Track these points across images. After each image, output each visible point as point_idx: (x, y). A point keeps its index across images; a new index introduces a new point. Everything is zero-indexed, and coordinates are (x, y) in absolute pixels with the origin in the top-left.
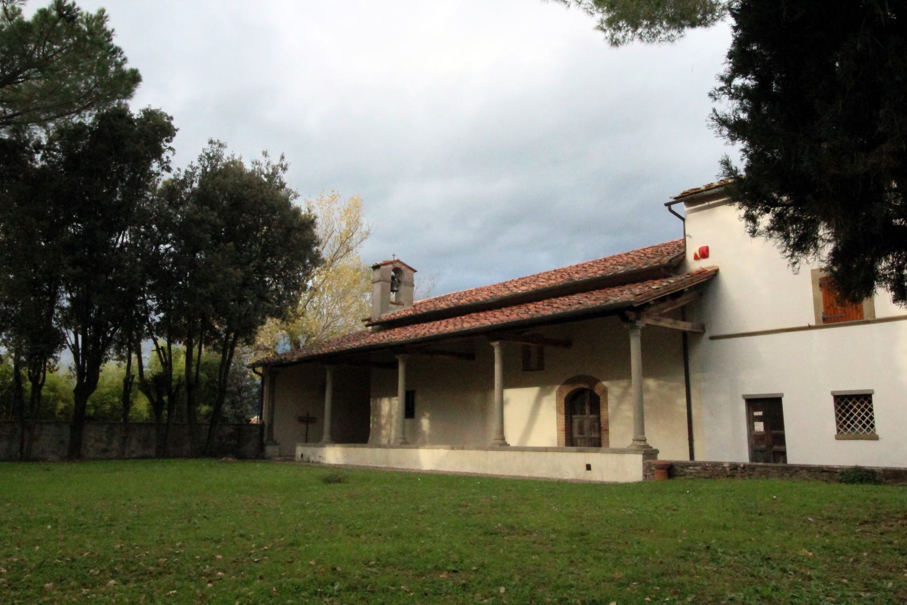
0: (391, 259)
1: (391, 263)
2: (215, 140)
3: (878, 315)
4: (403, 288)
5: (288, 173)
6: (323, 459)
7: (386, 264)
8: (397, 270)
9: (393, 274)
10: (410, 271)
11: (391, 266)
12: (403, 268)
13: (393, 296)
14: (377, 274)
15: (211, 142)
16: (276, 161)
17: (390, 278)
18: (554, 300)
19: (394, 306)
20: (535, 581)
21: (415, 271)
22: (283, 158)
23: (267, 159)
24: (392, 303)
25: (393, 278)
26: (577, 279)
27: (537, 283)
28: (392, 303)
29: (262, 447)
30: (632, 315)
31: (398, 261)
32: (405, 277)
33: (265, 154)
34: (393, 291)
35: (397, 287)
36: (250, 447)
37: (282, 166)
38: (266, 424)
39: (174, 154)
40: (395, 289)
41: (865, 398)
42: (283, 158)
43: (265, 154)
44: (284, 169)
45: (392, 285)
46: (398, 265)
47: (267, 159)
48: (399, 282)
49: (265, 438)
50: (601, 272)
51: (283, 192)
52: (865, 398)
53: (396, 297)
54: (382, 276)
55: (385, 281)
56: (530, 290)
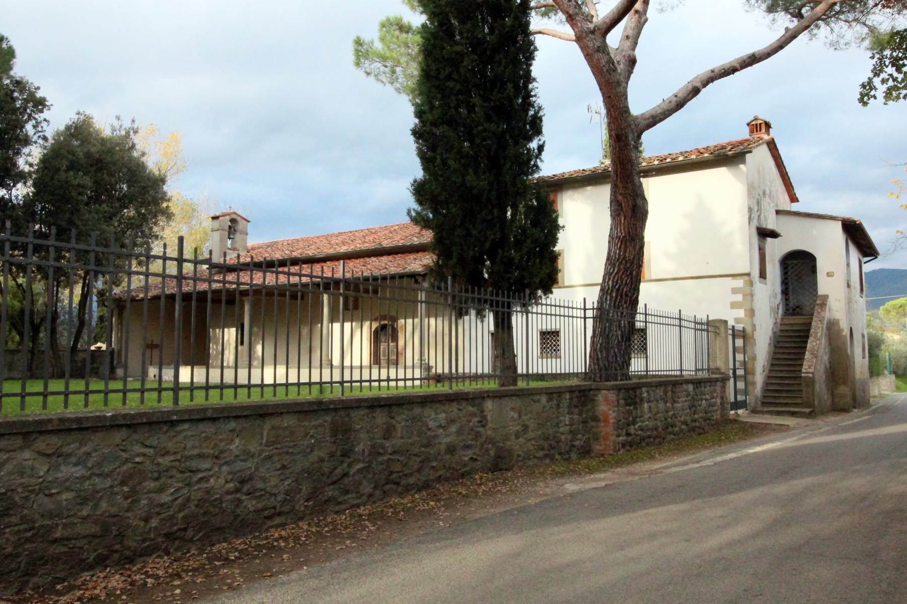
0: (228, 211)
1: (228, 214)
2: (81, 111)
3: (566, 284)
4: (238, 237)
5: (137, 135)
6: (801, 309)
7: (223, 216)
8: (233, 221)
9: (230, 223)
10: (245, 222)
11: (228, 218)
12: (239, 219)
13: (229, 242)
14: (216, 224)
15: (78, 113)
16: (127, 124)
17: (228, 228)
18: (367, 259)
19: (230, 251)
20: (439, 149)
21: (249, 222)
22: (133, 121)
23: (120, 123)
24: (229, 249)
25: (230, 227)
26: (385, 246)
27: (355, 243)
28: (229, 249)
29: (112, 369)
30: (420, 279)
31: (235, 213)
32: (241, 225)
33: (118, 118)
34: (230, 238)
35: (234, 234)
36: (105, 369)
37: (133, 129)
38: (116, 350)
39: (48, 125)
40: (232, 237)
41: (556, 333)
42: (133, 121)
43: (118, 118)
44: (136, 132)
45: (229, 233)
46: (234, 216)
47: (120, 123)
48: (235, 230)
49: (115, 362)
50: (402, 241)
51: (135, 154)
52: (556, 333)
53: (232, 244)
54: (220, 226)
55: (223, 230)
56: (350, 250)
